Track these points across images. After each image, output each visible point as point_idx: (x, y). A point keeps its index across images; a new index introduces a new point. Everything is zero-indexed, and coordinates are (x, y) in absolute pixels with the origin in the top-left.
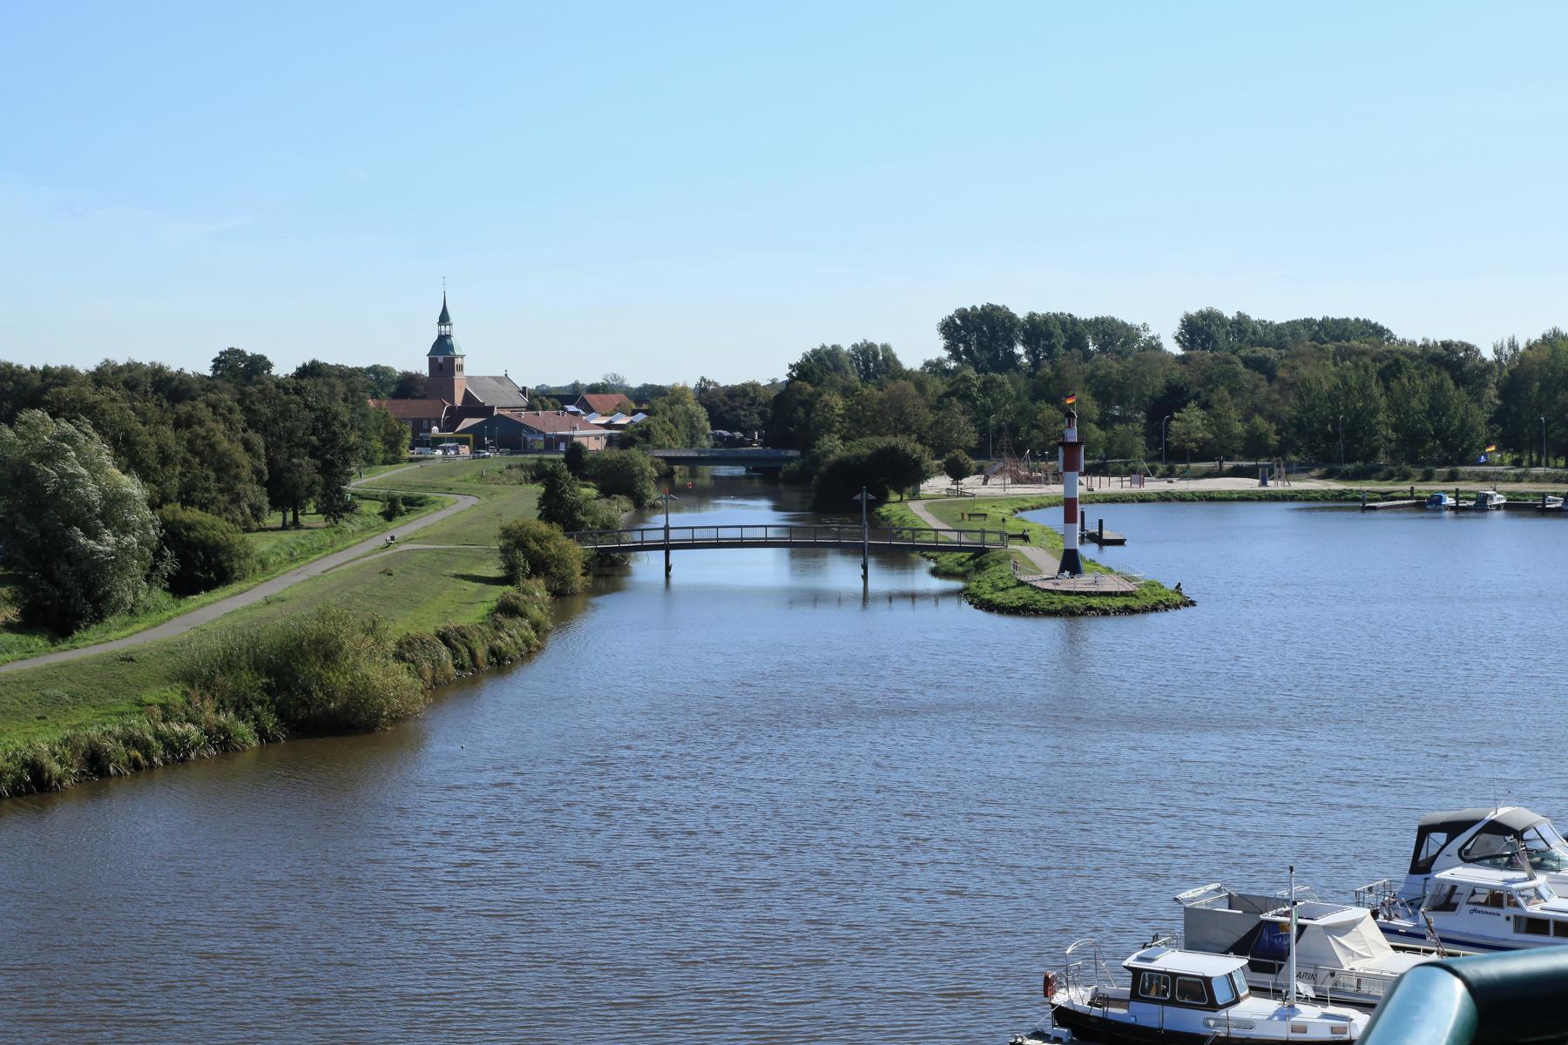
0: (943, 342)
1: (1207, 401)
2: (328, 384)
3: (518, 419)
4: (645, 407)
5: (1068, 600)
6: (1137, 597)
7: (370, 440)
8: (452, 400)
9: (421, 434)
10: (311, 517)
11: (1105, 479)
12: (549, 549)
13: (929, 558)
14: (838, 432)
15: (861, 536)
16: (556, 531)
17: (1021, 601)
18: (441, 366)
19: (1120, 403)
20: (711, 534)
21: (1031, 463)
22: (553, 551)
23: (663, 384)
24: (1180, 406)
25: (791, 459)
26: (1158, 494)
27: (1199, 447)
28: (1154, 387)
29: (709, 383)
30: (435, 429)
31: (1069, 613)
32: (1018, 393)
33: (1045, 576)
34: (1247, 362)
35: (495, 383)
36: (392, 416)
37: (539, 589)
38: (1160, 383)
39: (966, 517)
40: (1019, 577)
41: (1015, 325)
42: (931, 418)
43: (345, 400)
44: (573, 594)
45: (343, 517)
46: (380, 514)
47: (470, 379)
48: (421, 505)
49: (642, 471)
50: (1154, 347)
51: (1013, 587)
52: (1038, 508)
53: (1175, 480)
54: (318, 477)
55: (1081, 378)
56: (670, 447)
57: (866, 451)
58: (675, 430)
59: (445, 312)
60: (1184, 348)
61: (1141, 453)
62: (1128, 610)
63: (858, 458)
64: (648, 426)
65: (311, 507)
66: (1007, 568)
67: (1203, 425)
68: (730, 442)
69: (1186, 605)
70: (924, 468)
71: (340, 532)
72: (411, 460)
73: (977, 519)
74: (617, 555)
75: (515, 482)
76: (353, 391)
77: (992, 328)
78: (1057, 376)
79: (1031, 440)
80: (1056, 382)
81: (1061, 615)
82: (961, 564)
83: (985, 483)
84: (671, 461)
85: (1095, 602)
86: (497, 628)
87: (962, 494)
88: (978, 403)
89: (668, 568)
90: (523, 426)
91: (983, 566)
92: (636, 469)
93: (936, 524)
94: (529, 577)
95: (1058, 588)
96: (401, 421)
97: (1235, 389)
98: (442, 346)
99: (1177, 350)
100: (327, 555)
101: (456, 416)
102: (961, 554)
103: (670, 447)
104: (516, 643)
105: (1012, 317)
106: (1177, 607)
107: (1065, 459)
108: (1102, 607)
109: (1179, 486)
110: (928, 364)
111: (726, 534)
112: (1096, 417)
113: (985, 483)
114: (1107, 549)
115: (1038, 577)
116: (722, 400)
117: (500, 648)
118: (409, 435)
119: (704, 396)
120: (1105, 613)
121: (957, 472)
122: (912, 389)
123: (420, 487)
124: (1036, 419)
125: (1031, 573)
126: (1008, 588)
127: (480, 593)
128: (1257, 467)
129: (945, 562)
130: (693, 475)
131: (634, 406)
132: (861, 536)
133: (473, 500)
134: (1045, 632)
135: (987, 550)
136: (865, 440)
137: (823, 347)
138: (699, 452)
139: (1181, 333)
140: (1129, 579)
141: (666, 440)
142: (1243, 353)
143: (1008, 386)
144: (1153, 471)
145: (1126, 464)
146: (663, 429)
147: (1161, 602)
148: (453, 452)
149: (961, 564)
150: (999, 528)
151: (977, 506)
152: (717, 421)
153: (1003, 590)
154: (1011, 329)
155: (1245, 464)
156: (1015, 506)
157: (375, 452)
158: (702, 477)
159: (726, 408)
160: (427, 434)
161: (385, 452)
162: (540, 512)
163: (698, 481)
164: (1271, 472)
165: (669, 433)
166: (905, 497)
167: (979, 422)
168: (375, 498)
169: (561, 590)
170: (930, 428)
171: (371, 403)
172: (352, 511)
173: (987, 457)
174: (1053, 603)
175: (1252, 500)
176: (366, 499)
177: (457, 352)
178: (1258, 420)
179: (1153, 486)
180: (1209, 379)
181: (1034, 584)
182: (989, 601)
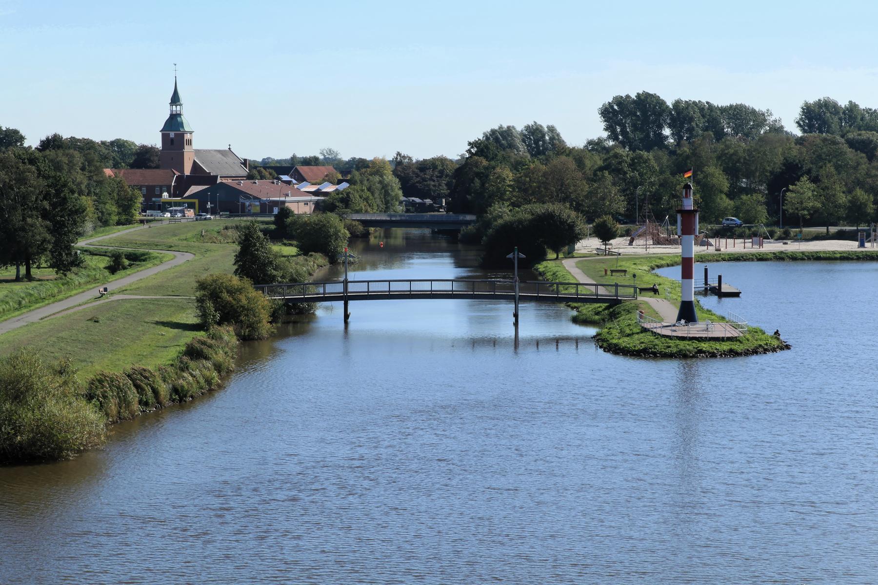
0: (603, 125)
1: (818, 175)
2: (67, 155)
3: (237, 187)
4: (349, 177)
5: (682, 345)
6: (741, 342)
7: (105, 204)
8: (181, 170)
9: (154, 199)
10: (44, 271)
11: (730, 241)
12: (240, 300)
13: (573, 308)
14: (509, 199)
15: (512, 288)
16: (247, 283)
17: (642, 345)
18: (172, 140)
19: (747, 178)
20: (405, 287)
21: (669, 227)
22: (244, 302)
23: (94, 140)
24: (795, 180)
25: (468, 223)
26: (774, 253)
27: (810, 214)
28: (775, 163)
29: (404, 157)
30: (165, 195)
31: (683, 355)
32: (661, 169)
33: (665, 324)
34: (851, 144)
35: (220, 156)
36: (126, 184)
37: (228, 334)
38: (779, 160)
39: (609, 273)
40: (643, 325)
41: (664, 111)
42: (587, 188)
43: (83, 169)
44: (260, 339)
45: (70, 270)
46: (105, 268)
47: (197, 152)
48: (144, 260)
49: (336, 233)
50: (777, 129)
51: (638, 333)
52: (672, 265)
53: (789, 242)
54: (48, 237)
55: (714, 155)
56: (366, 211)
57: (529, 217)
58: (371, 197)
59: (176, 93)
60: (804, 131)
61: (764, 221)
62: (733, 353)
63: (520, 222)
64: (348, 194)
65: (43, 260)
66: (636, 315)
67: (813, 195)
68: (422, 208)
69: (782, 349)
70: (577, 231)
71: (67, 283)
72: (142, 222)
73: (618, 274)
74: (305, 305)
75: (229, 241)
76: (90, 162)
77: (644, 112)
78: (694, 154)
79: (671, 208)
80: (693, 159)
81: (676, 357)
82: (597, 313)
83: (631, 243)
84: (366, 223)
85: (705, 346)
86: (182, 370)
87: (611, 254)
88: (628, 176)
89: (346, 316)
90: (241, 192)
91: (615, 315)
92: (332, 230)
93: (582, 279)
94: (220, 323)
95: (674, 334)
96: (133, 187)
97: (841, 166)
98: (174, 123)
99: (798, 133)
100: (49, 304)
101: (183, 183)
102: (599, 305)
103: (366, 211)
104: (198, 382)
105: (662, 103)
106: (774, 350)
107: (683, 224)
108: (711, 350)
109: (793, 247)
110: (590, 143)
111: (417, 287)
112: (726, 189)
113: (631, 243)
114: (726, 300)
115: (659, 325)
116: (413, 172)
117: (182, 387)
118: (141, 199)
119: (399, 168)
120: (713, 355)
121: (605, 234)
122: (572, 165)
123: (145, 244)
124: (675, 190)
125: (652, 321)
126: (633, 334)
127: (175, 338)
128: (858, 231)
129: (584, 311)
130: (387, 235)
131: (340, 177)
132: (512, 288)
133: (189, 257)
134: (670, 370)
135: (619, 302)
136: (528, 207)
137: (501, 127)
138: (390, 216)
139: (801, 119)
140: (736, 327)
141: (363, 205)
142: (850, 136)
143: (653, 162)
144: (772, 235)
145: (749, 228)
146: (361, 197)
147: (760, 346)
148: (179, 215)
149: (597, 313)
150: (631, 283)
151: (620, 263)
152: (408, 189)
153: (628, 335)
154: (660, 114)
155: (848, 228)
156: (653, 264)
157: (110, 214)
158: (395, 238)
159: (418, 179)
160: (158, 199)
161: (119, 214)
162: (236, 267)
163: (392, 241)
164: (868, 236)
165: (366, 199)
166: (561, 256)
167: (628, 192)
168: (104, 254)
169: (249, 336)
170: (586, 197)
171: (108, 172)
172: (78, 265)
173: (633, 222)
174: (669, 347)
175: (852, 259)
176: (96, 255)
177: (186, 129)
178: (859, 193)
179: (771, 247)
180: (819, 157)
181: (655, 330)
182: (616, 345)
